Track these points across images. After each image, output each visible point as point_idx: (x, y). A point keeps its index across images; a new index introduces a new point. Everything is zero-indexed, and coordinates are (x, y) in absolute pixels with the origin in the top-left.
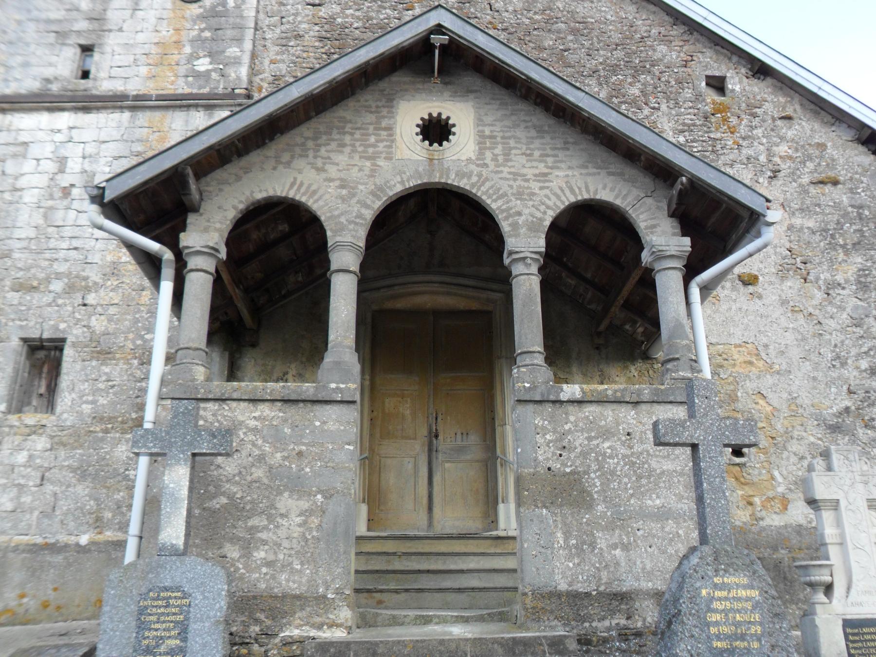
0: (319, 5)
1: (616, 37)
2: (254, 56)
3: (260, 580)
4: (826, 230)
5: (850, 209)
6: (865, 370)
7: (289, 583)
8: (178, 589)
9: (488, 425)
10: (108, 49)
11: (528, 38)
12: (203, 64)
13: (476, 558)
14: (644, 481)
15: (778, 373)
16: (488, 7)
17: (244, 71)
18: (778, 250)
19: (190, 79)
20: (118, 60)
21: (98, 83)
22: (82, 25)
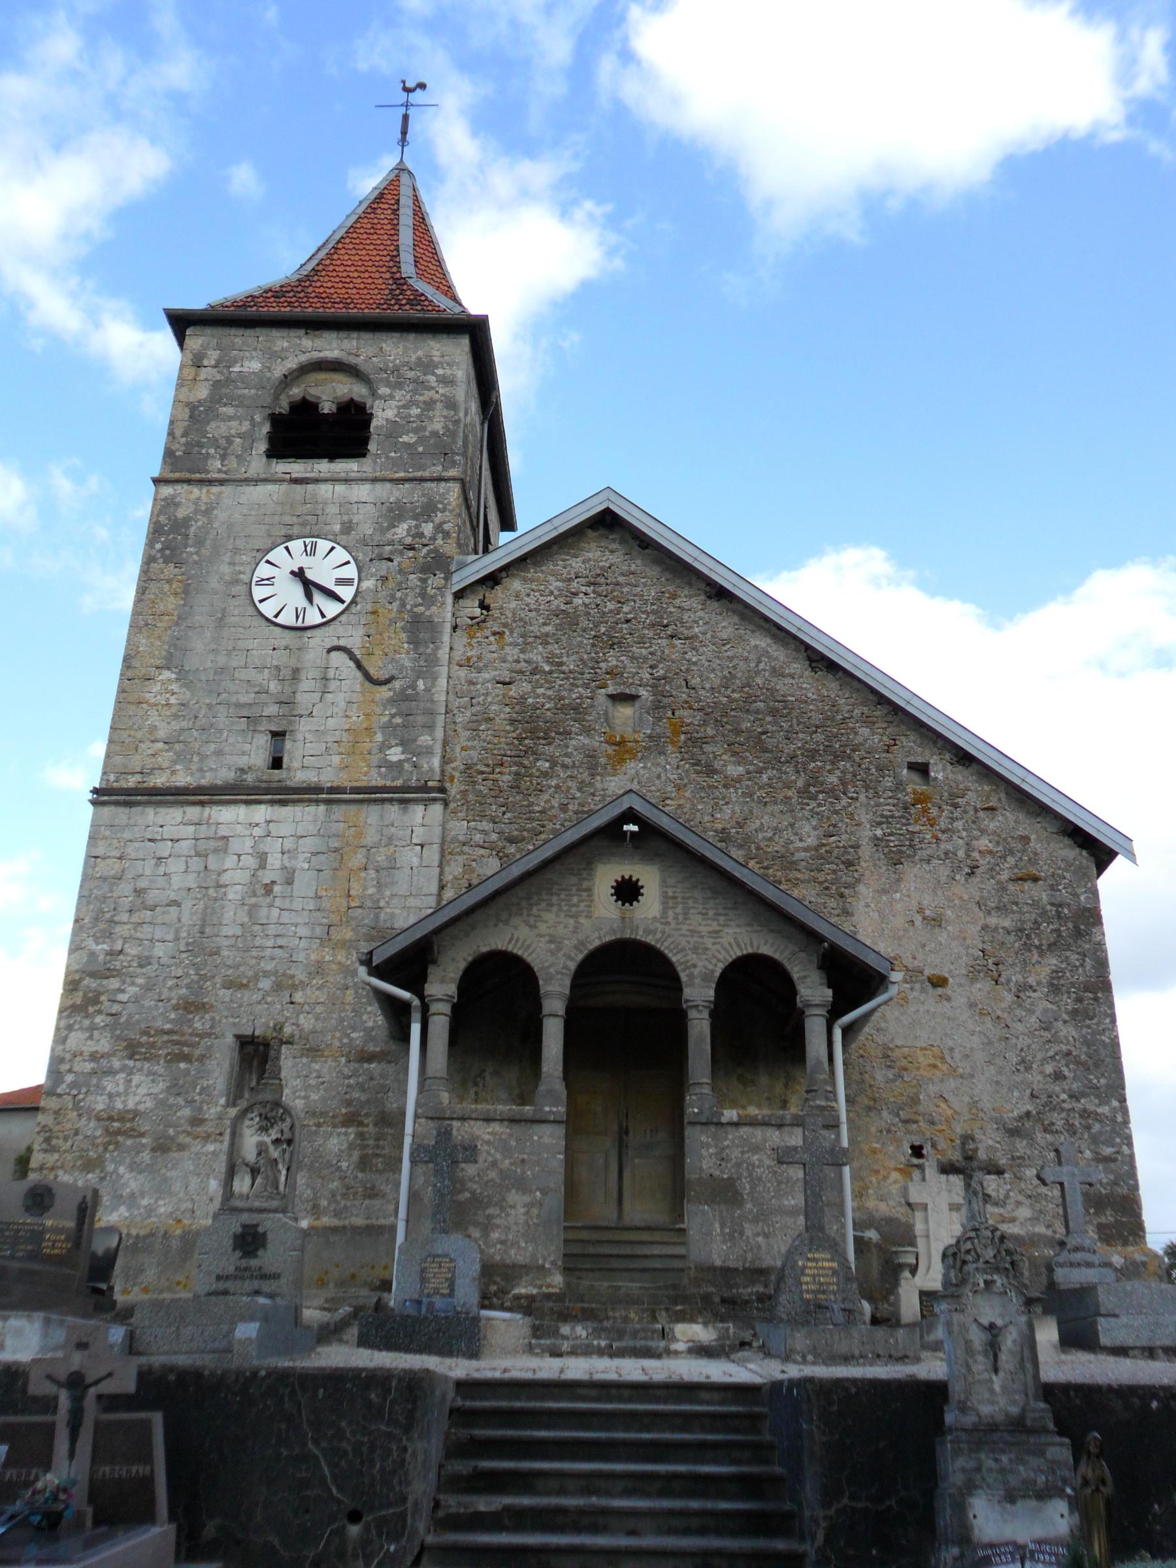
0: (510, 683)
1: (817, 718)
2: (445, 743)
3: (497, 1254)
4: (1021, 930)
5: (1049, 907)
6: (1049, 1076)
7: (516, 1256)
8: (447, 1256)
9: (676, 1124)
10: (300, 737)
11: (725, 720)
12: (395, 754)
13: (659, 1246)
14: (783, 1186)
15: (961, 1076)
16: (684, 683)
17: (436, 762)
18: (970, 951)
19: (383, 770)
20: (311, 748)
21: (292, 774)
22: (272, 710)
